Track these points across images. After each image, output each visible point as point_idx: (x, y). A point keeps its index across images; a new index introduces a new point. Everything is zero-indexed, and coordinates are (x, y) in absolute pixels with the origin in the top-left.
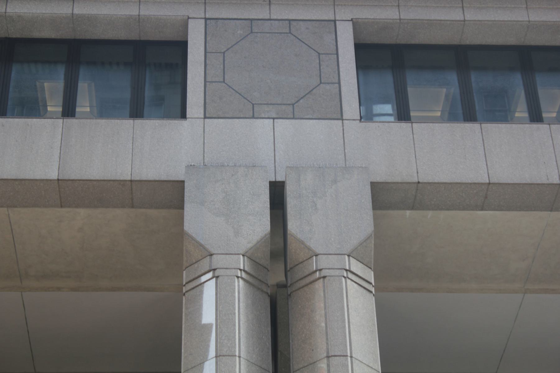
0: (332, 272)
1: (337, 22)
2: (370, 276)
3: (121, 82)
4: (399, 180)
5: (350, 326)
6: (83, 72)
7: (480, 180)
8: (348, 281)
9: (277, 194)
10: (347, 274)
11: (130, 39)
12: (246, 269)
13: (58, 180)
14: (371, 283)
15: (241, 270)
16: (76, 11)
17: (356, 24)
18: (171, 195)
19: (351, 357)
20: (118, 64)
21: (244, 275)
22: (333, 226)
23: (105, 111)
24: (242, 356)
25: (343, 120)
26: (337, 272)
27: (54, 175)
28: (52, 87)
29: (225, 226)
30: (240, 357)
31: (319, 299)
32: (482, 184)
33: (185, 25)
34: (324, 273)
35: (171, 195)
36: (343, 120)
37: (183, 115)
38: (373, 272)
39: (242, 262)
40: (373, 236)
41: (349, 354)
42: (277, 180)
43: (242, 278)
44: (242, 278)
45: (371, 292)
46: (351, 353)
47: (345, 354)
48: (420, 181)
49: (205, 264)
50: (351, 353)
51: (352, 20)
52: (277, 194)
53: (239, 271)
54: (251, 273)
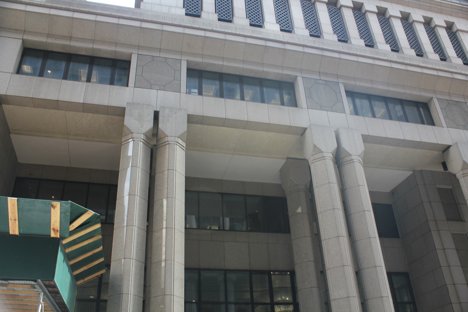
0: (172, 142)
2: (184, 145)
3: (107, 72)
4: (197, 114)
6: (72, 64)
9: (156, 115)
16: (117, 50)
17: (188, 62)
18: (120, 112)
21: (143, 141)
22: (173, 127)
27: (81, 101)
29: (138, 124)
33: (296, 77)
34: (169, 142)
35: (120, 112)
37: (127, 86)
39: (142, 136)
42: (227, 117)
52: (156, 115)
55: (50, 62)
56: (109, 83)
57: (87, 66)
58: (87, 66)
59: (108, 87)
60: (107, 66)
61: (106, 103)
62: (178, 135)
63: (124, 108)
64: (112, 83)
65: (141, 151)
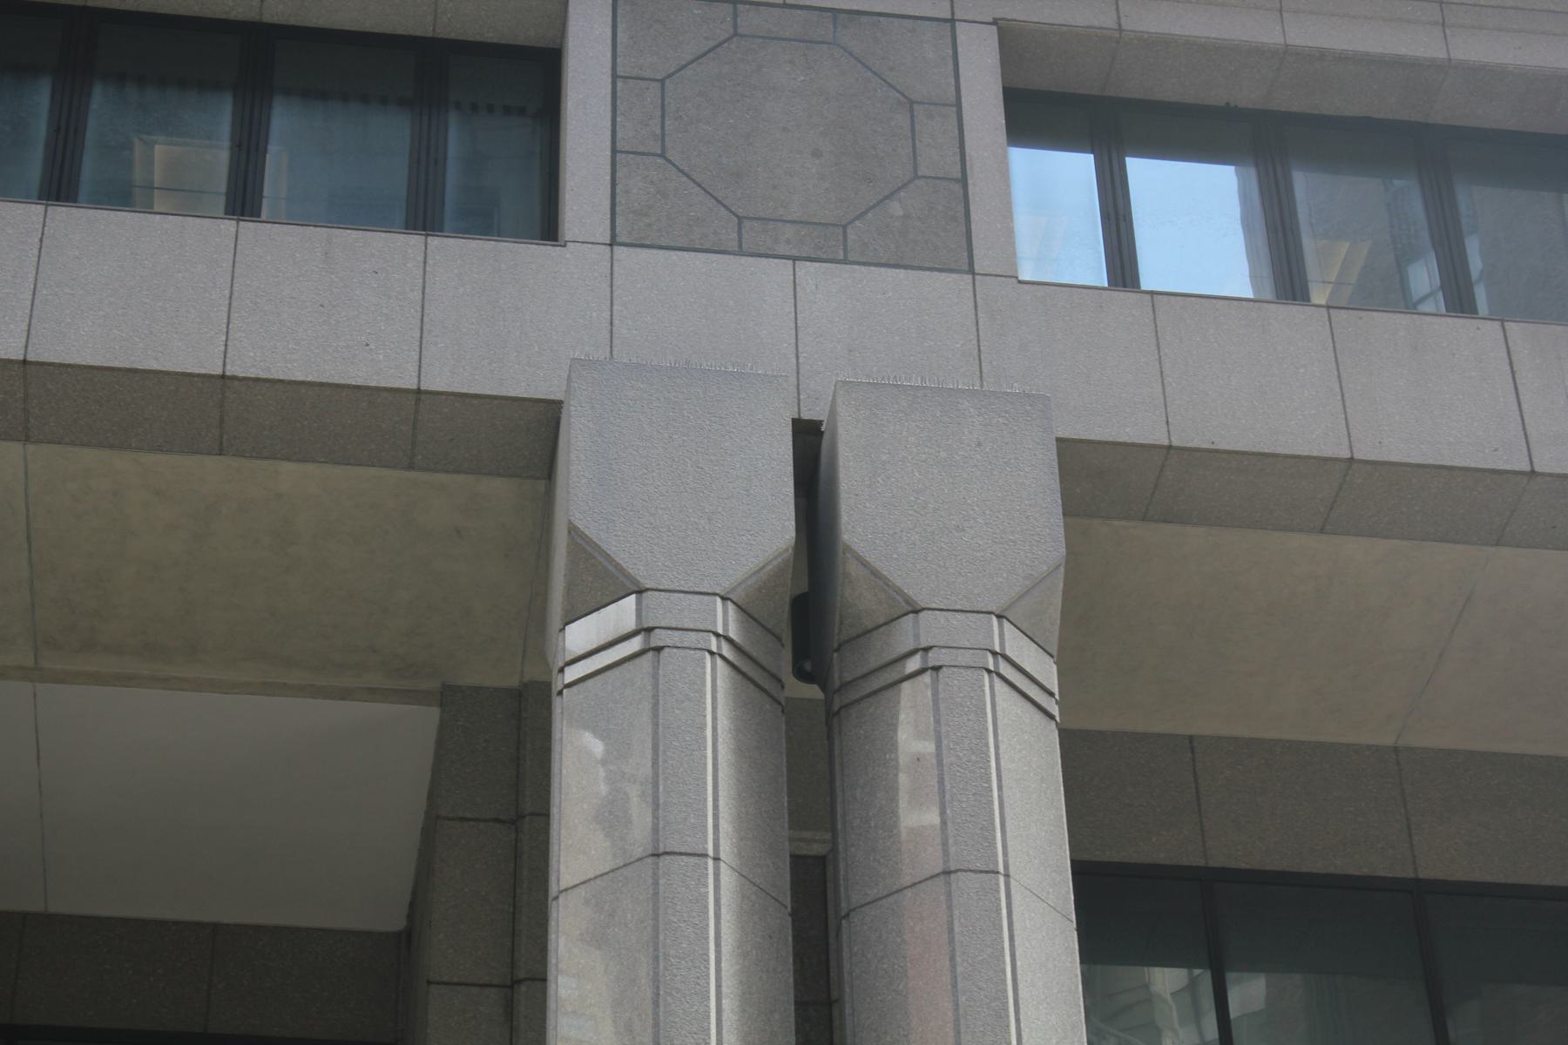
1: (960, 27)
2: (1048, 673)
5: (988, 799)
6: (100, 101)
7: (1328, 451)
8: (997, 682)
9: (810, 442)
10: (996, 664)
11: (400, 32)
12: (732, 635)
13: (419, 391)
14: (1052, 694)
15: (717, 635)
18: (527, 439)
19: (1007, 876)
20: (491, 109)
21: (726, 651)
22: (961, 534)
23: (352, 210)
24: (723, 856)
25: (974, 274)
26: (965, 658)
28: (201, 143)
29: (673, 529)
30: (717, 859)
31: (912, 726)
32: (1337, 459)
34: (934, 658)
35: (527, 439)
36: (974, 274)
37: (549, 229)
38: (1055, 668)
39: (725, 619)
40: (1062, 569)
41: (711, 853)
43: (722, 656)
44: (722, 656)
45: (1052, 717)
46: (1006, 867)
47: (991, 867)
48: (1357, 456)
49: (905, 635)
50: (1006, 867)
51: (995, 22)
52: (810, 442)
53: (714, 639)
54: (748, 648)
55: (287, 125)
56: (221, 213)
57: (221, 116)
58: (221, 116)
59: (395, 252)
60: (491, 109)
61: (388, 367)
62: (724, 585)
63: (560, 403)
64: (423, 215)
65: (724, 723)
